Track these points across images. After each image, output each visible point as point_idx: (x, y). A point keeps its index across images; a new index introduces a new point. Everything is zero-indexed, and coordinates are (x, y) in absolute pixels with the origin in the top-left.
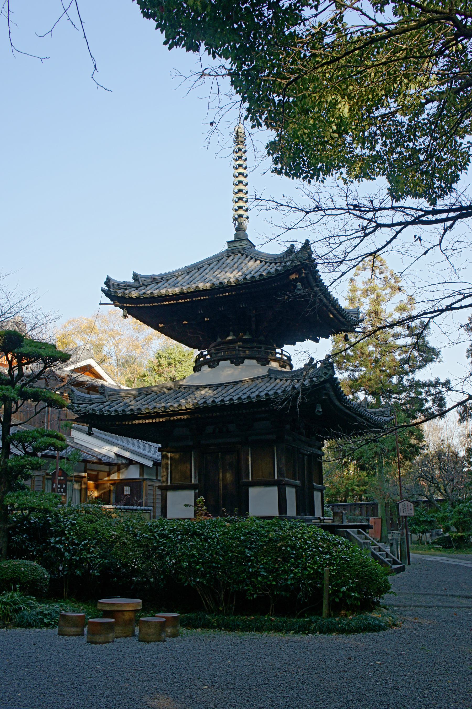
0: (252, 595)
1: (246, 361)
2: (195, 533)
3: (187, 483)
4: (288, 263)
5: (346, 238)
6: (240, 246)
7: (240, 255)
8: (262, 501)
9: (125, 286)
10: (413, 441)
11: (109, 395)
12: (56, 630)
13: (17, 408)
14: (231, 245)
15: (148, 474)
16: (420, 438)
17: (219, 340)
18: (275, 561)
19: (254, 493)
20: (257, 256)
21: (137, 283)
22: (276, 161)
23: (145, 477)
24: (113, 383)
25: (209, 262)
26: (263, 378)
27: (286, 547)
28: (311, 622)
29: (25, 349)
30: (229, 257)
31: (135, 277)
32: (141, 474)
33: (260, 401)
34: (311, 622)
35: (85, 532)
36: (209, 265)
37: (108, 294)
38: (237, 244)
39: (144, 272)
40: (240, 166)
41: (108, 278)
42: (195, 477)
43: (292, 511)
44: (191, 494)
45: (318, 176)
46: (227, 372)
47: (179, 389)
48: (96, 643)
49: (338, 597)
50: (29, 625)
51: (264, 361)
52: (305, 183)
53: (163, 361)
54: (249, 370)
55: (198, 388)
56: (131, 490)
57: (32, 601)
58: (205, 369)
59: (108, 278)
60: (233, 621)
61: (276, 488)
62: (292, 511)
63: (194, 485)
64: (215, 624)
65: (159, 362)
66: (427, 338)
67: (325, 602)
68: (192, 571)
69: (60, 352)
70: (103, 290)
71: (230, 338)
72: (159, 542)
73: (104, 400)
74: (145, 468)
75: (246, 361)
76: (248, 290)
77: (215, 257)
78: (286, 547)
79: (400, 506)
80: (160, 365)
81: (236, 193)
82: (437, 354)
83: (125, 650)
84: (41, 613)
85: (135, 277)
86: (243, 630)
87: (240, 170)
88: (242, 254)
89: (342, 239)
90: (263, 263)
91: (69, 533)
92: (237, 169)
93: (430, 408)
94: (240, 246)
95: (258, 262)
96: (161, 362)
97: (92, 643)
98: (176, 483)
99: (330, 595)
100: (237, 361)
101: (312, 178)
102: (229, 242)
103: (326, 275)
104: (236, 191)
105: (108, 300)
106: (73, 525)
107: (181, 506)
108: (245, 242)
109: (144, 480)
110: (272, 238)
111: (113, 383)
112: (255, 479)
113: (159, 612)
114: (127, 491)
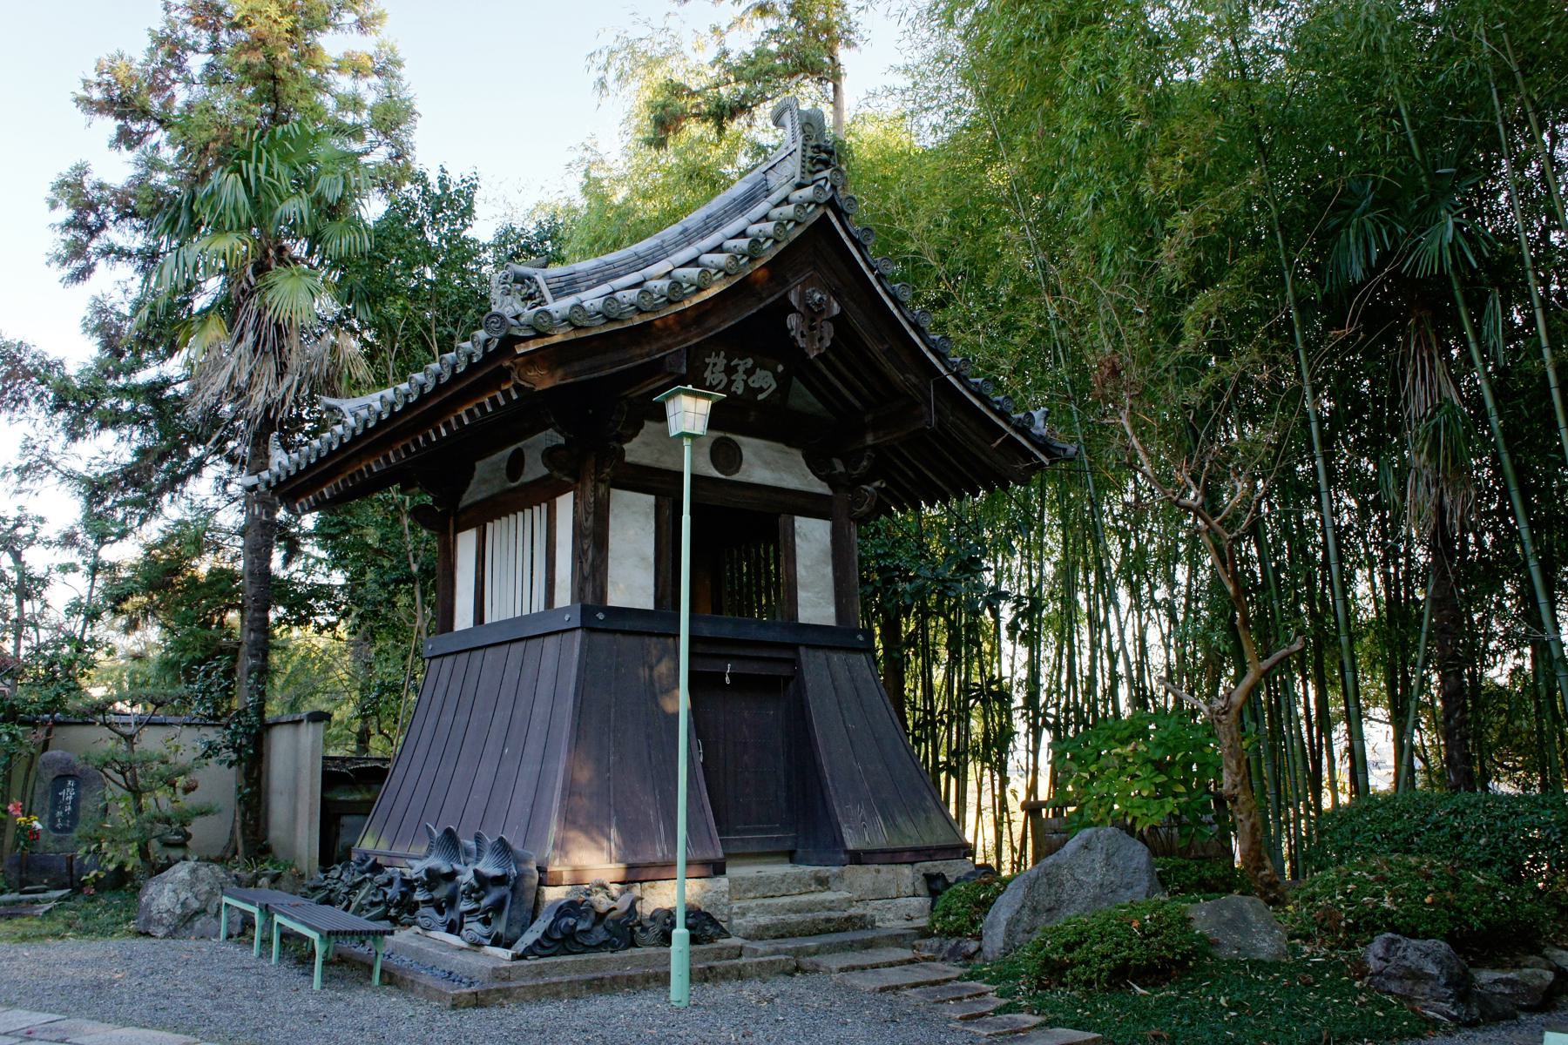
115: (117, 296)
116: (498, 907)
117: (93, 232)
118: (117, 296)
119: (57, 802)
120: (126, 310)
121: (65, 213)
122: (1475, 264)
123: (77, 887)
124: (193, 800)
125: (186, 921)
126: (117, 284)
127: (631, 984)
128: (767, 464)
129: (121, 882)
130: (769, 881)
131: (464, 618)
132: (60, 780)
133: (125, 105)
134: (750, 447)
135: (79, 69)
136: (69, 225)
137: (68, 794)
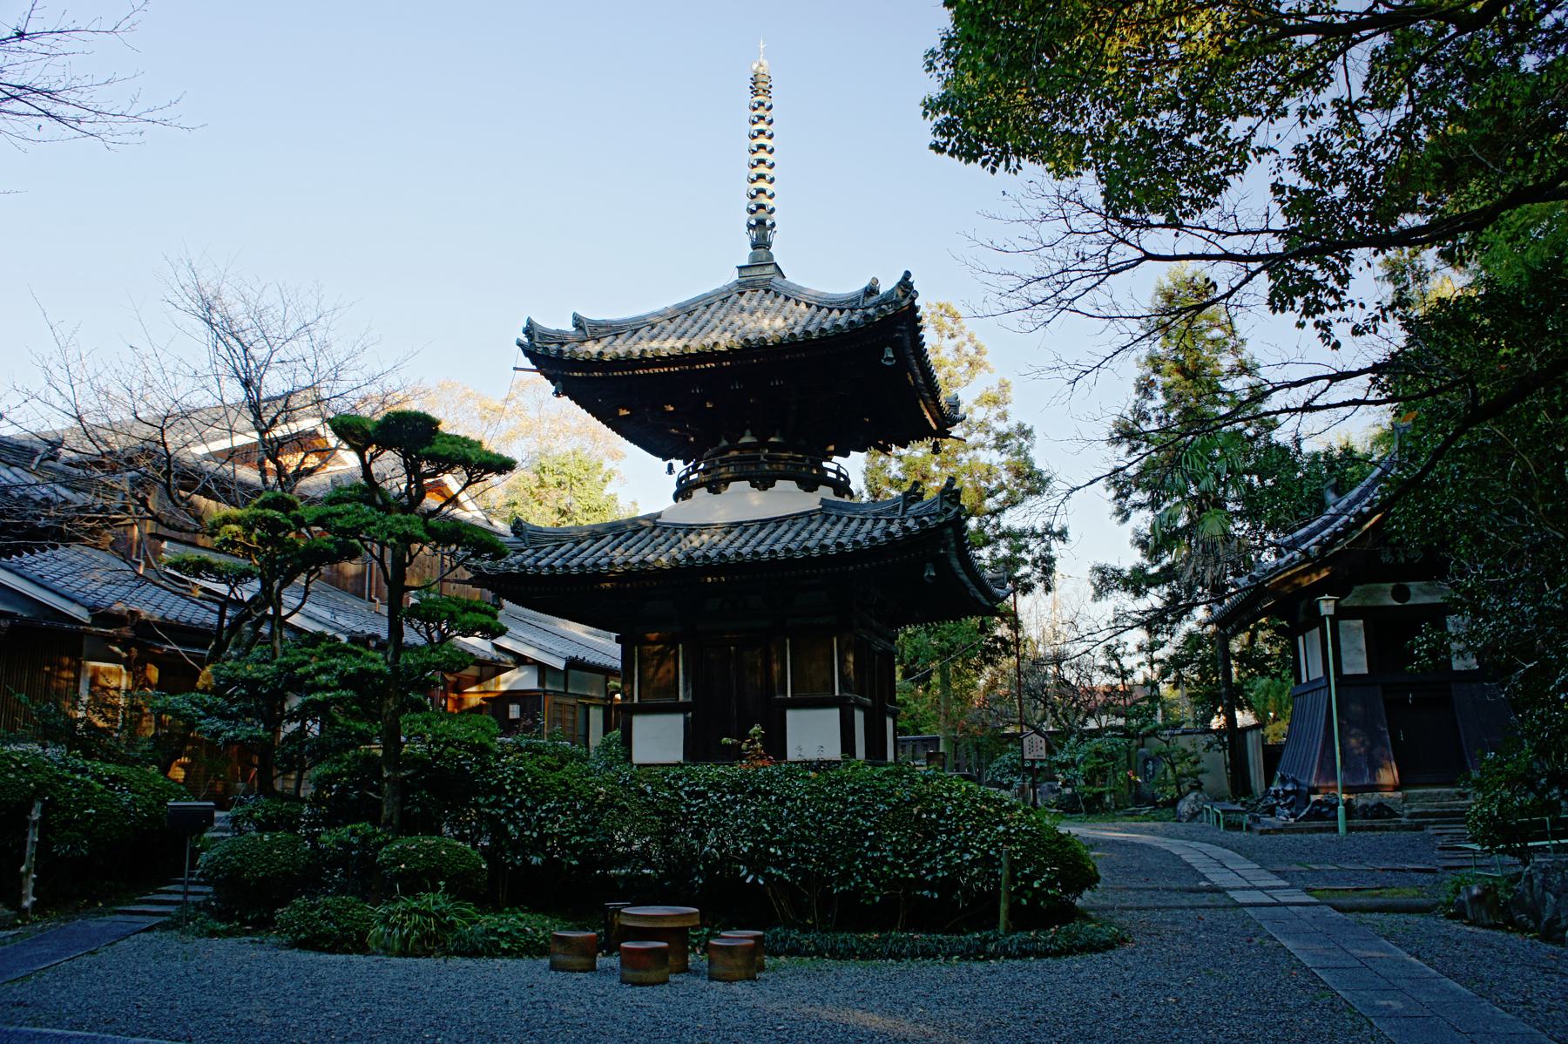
0: (872, 897)
1: (778, 483)
2: (757, 791)
3: (827, 695)
4: (871, 311)
5: (1078, 275)
6: (760, 276)
7: (762, 292)
8: (813, 735)
9: (561, 339)
10: (1002, 631)
11: (530, 536)
12: (547, 961)
13: (412, 558)
14: (745, 273)
15: (553, 683)
16: (1016, 625)
17: (724, 443)
18: (912, 839)
19: (795, 720)
20: (790, 296)
21: (581, 333)
22: (939, 129)
23: (548, 687)
24: (479, 514)
25: (707, 302)
26: (809, 515)
27: (929, 812)
28: (985, 941)
29: (439, 448)
30: (742, 294)
31: (578, 322)
32: (541, 682)
33: (792, 558)
34: (985, 941)
35: (544, 789)
36: (708, 306)
37: (529, 352)
38: (756, 272)
39: (593, 314)
40: (761, 132)
41: (530, 322)
42: (686, 690)
43: (860, 752)
44: (677, 721)
45: (1008, 161)
46: (743, 502)
47: (650, 527)
48: (641, 984)
49: (1025, 897)
50: (475, 953)
51: (809, 485)
52: (986, 172)
53: (550, 479)
54: (786, 498)
55: (689, 529)
56: (522, 711)
57: (469, 909)
58: (701, 494)
59: (530, 322)
60: (844, 941)
61: (836, 712)
62: (860, 752)
63: (683, 703)
64: (812, 948)
65: (541, 479)
66: (1032, 454)
67: (1004, 907)
68: (757, 860)
69: (488, 453)
70: (520, 344)
71: (743, 440)
72: (688, 806)
73: (522, 546)
74: (548, 675)
75: (778, 483)
76: (755, 357)
77: (717, 293)
78: (929, 812)
79: (1026, 741)
80: (542, 485)
81: (753, 181)
82: (1045, 482)
83: (695, 996)
84: (494, 931)
85: (578, 322)
86: (863, 957)
87: (762, 140)
88: (767, 291)
89: (1074, 275)
90: (814, 308)
91: (514, 790)
92: (754, 137)
93: (1028, 576)
94: (760, 276)
95: (803, 306)
96: (546, 479)
97: (634, 984)
98: (651, 701)
99: (1011, 894)
100: (763, 482)
101: (996, 164)
102: (740, 268)
103: (929, 337)
104: (754, 176)
105: (526, 363)
106: (520, 773)
107: (658, 740)
108: (771, 269)
109: (545, 692)
110: (829, 267)
111: (479, 514)
112: (797, 696)
113: (728, 929)
114: (514, 711)
115: (1143, 525)
116: (1292, 803)
117: (1127, 496)
118: (1143, 525)
119: (1146, 771)
120: (1148, 532)
121: (1113, 493)
122: (664, 944)
123: (1156, 806)
124: (1200, 766)
125: (1193, 816)
126: (1142, 520)
127: (1327, 830)
128: (1426, 593)
129: (1173, 803)
130: (1430, 795)
131: (1304, 680)
132: (1146, 762)
133: (1126, 434)
134: (1413, 586)
135: (1106, 428)
136: (1117, 497)
137: (1150, 767)
